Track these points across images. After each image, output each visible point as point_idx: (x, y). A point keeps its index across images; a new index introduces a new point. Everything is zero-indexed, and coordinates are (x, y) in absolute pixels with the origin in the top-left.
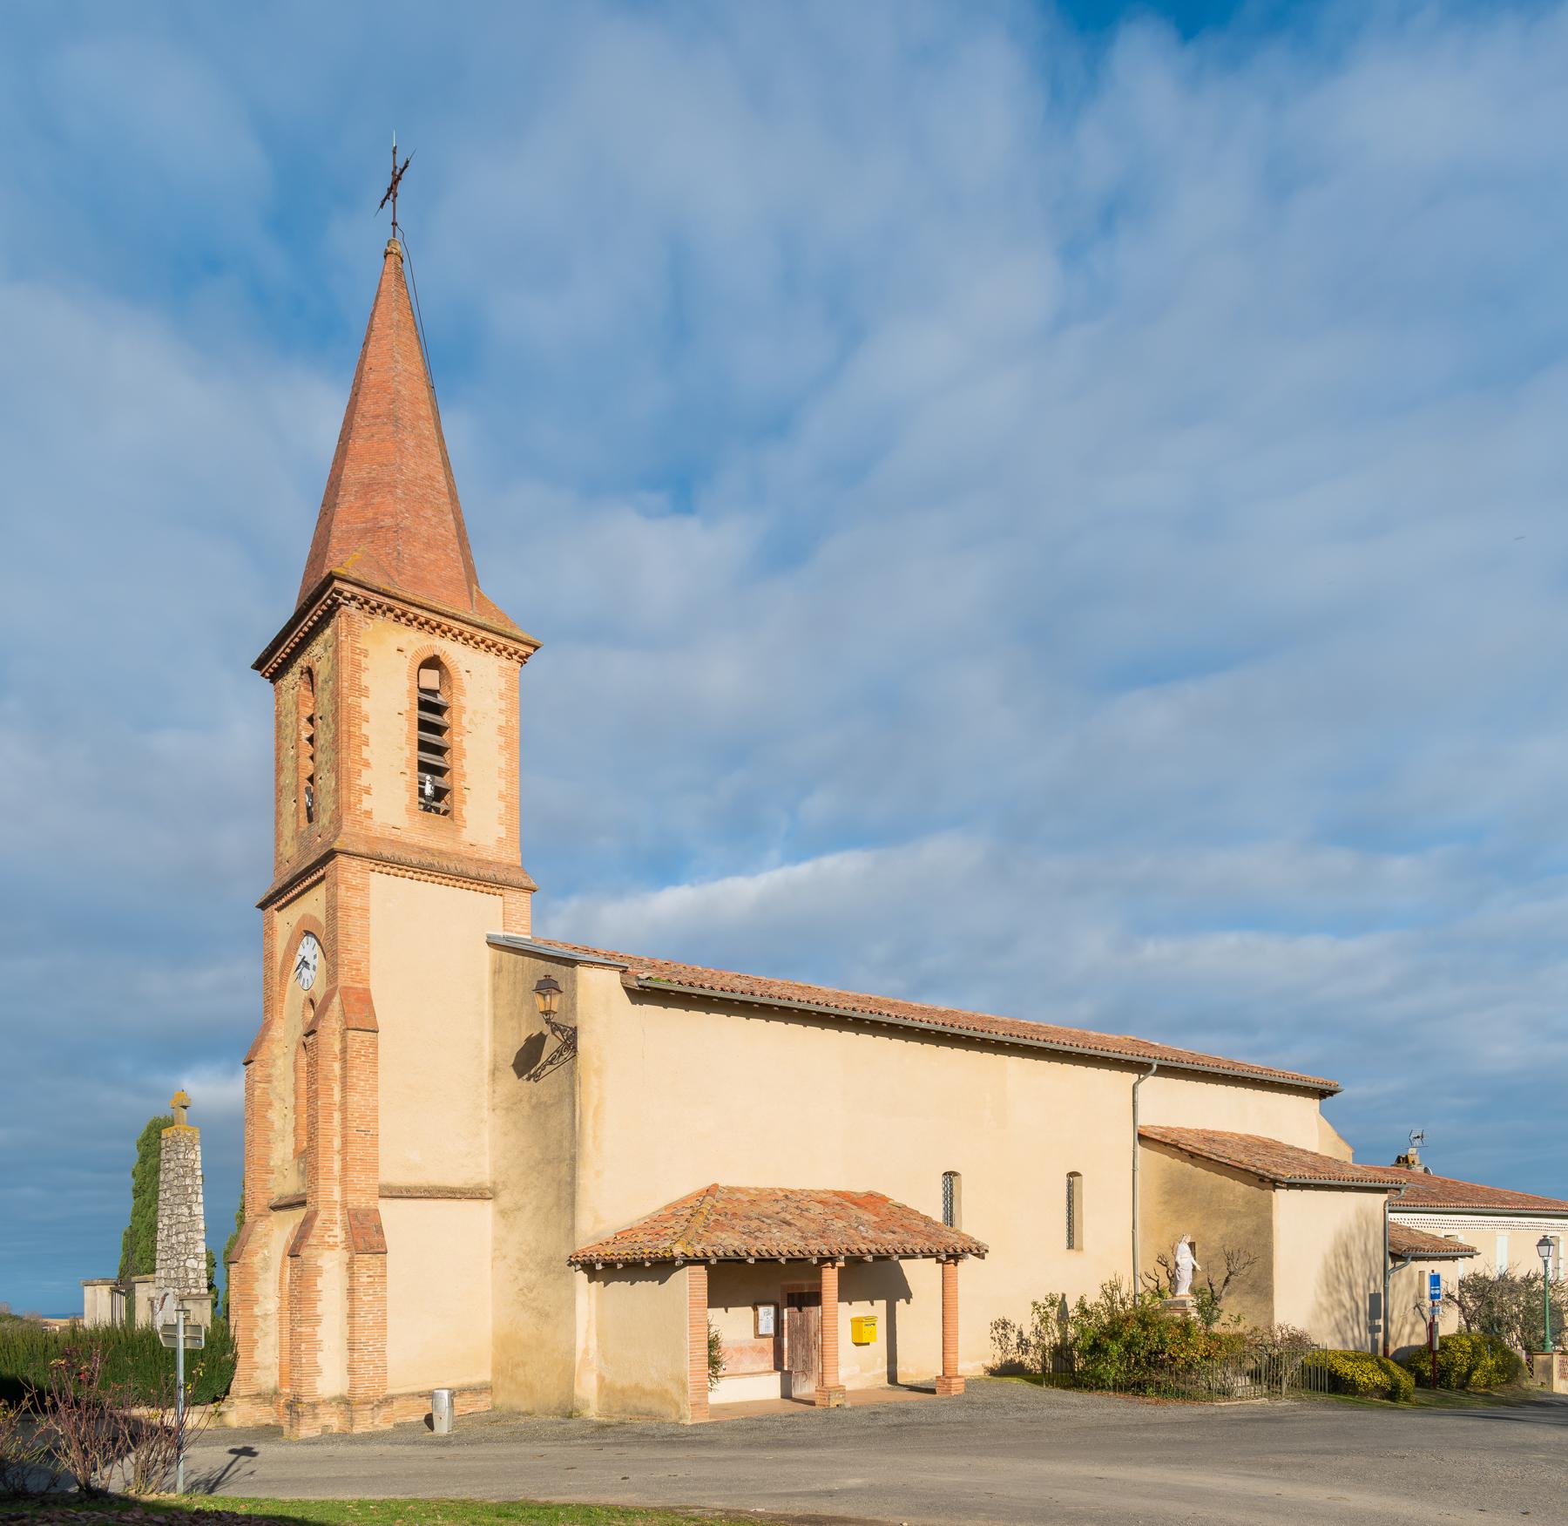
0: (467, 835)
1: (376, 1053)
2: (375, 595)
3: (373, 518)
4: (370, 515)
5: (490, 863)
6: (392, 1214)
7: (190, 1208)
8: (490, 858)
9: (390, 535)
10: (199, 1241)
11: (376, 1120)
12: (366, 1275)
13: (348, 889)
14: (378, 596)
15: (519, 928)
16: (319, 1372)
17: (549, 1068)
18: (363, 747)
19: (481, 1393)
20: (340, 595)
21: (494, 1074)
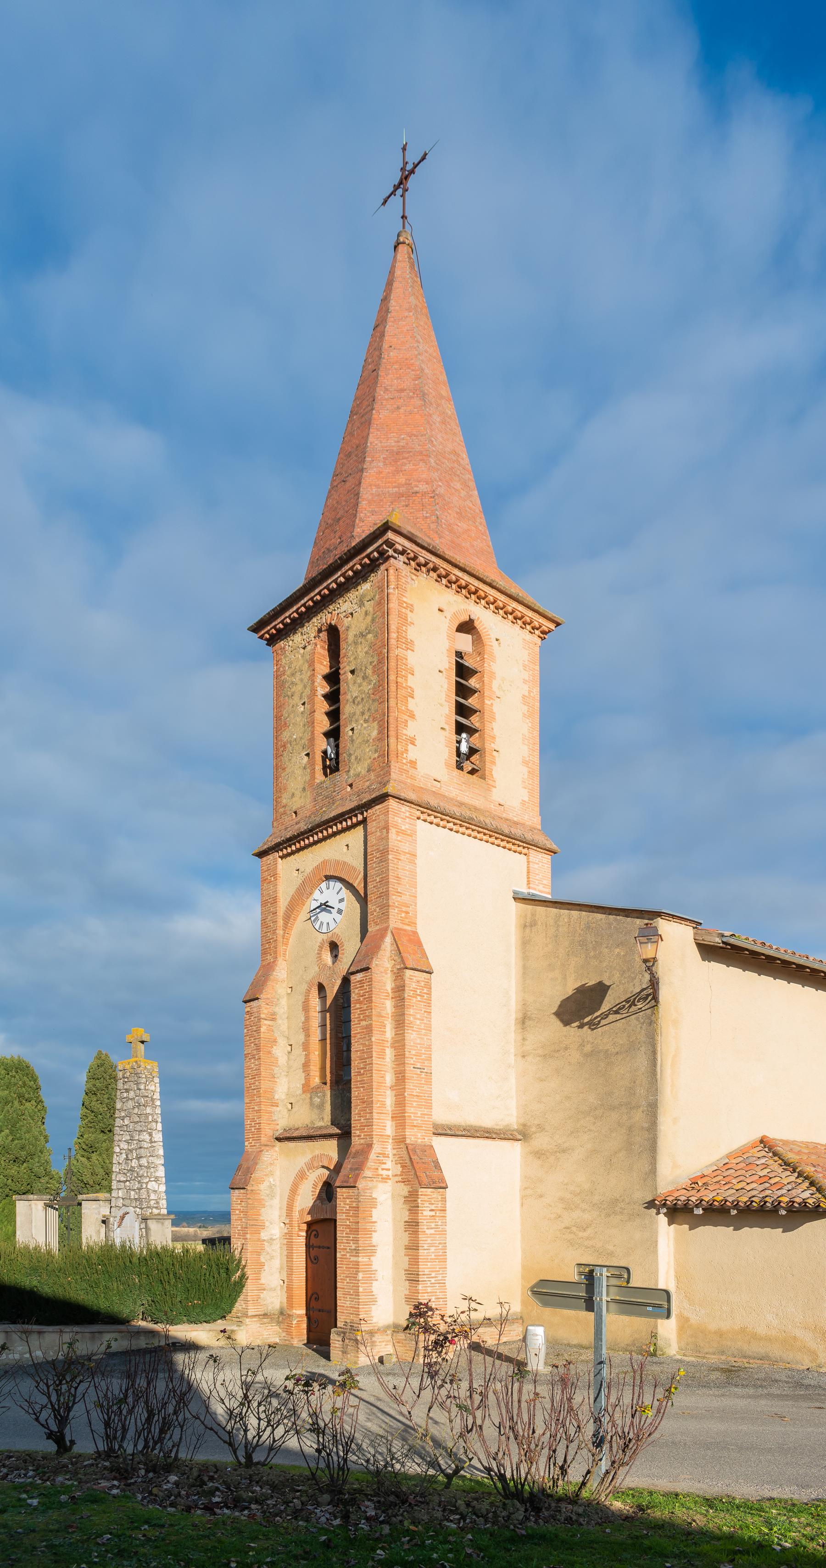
0: (497, 795)
1: (429, 994)
2: (424, 552)
3: (406, 484)
4: (402, 480)
5: (516, 823)
6: (443, 1147)
7: (150, 1135)
8: (515, 819)
9: (425, 500)
10: (159, 1166)
11: (429, 1059)
12: (429, 1209)
13: (398, 833)
14: (426, 553)
15: (541, 887)
16: (374, 1301)
17: (612, 1017)
18: (409, 699)
19: (513, 1323)
20: (391, 548)
21: (523, 1023)
